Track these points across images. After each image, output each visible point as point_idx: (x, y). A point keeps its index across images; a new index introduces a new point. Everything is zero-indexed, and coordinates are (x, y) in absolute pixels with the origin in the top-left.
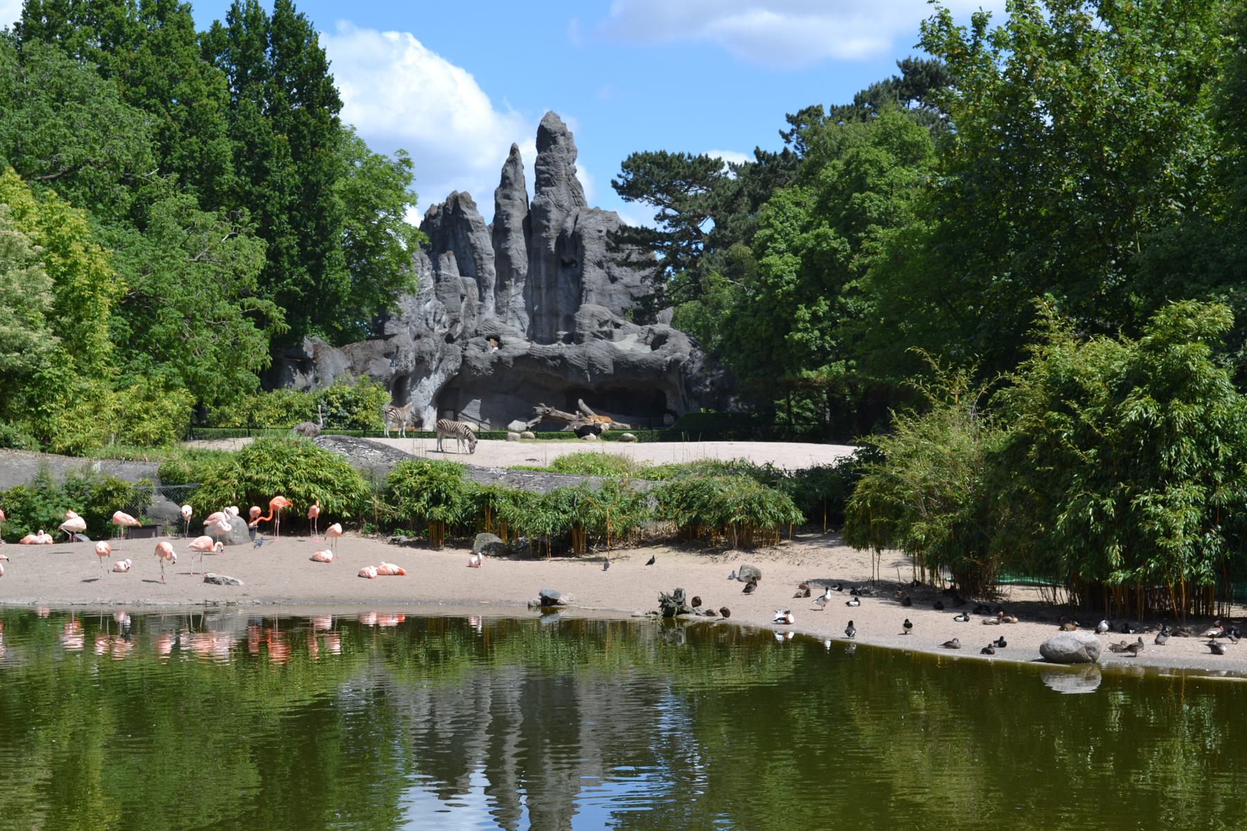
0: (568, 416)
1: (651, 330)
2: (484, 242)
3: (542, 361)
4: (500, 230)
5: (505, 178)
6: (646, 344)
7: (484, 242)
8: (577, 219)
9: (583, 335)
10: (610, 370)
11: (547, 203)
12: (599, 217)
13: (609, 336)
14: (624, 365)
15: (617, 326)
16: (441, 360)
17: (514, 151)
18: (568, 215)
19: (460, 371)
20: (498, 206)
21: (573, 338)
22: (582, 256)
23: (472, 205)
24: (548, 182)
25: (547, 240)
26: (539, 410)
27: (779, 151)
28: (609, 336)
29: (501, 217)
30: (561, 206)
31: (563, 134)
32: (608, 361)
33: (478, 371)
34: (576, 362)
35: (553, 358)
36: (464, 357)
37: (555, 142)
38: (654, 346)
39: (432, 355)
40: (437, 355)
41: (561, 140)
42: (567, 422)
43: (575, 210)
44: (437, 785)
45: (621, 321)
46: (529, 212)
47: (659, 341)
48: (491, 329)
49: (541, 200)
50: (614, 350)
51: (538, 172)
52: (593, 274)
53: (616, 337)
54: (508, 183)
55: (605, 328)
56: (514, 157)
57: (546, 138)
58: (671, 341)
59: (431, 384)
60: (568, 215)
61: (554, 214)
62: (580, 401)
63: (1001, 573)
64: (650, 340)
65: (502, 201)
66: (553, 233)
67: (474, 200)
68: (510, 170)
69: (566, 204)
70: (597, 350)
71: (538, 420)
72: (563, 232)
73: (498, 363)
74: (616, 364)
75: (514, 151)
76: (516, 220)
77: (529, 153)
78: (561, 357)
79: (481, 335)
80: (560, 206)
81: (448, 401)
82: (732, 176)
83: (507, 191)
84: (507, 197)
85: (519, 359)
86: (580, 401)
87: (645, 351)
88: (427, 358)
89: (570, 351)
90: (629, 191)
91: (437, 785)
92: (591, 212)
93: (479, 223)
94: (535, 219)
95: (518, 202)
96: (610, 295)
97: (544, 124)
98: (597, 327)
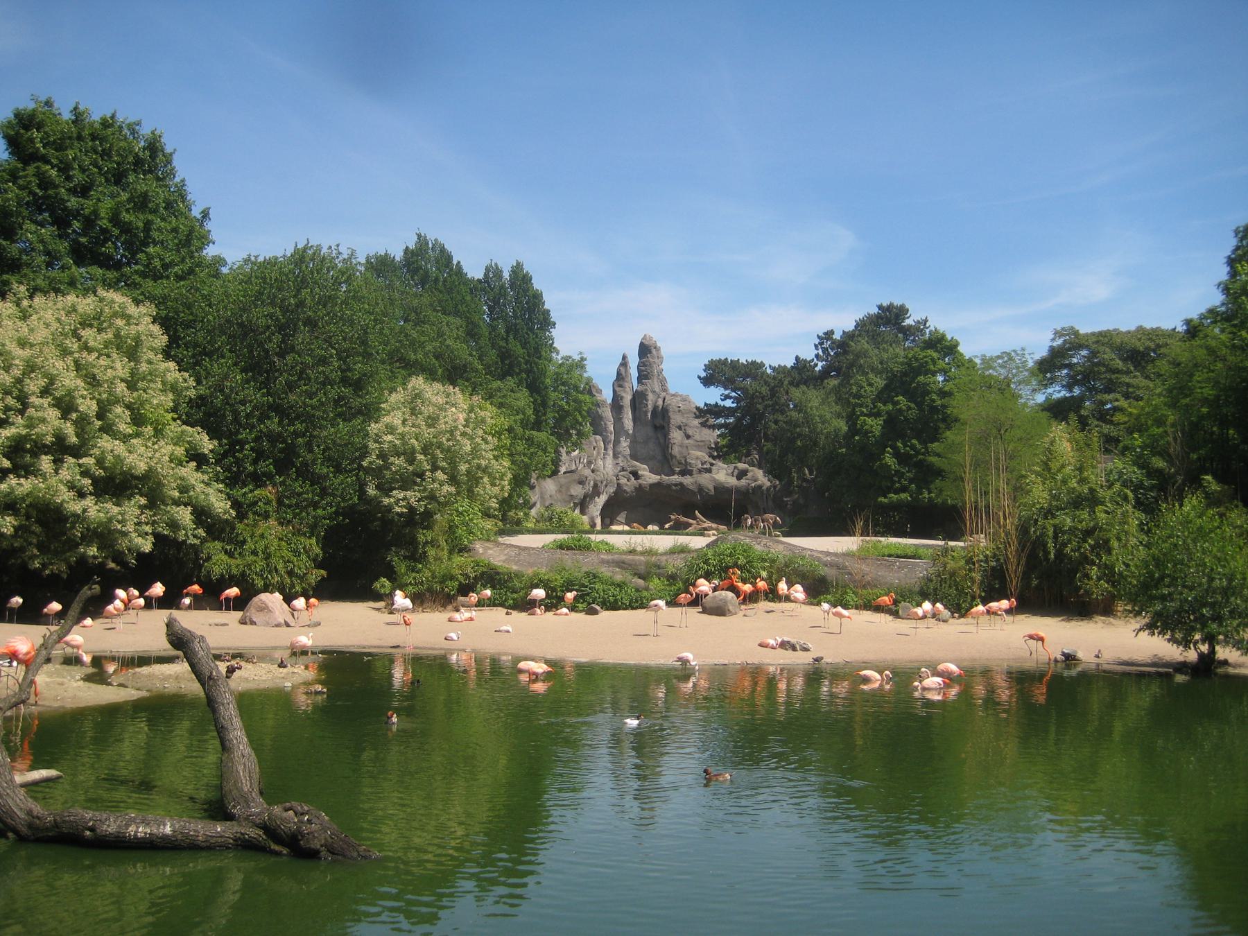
0: (691, 521)
1: (735, 468)
2: (607, 413)
3: (669, 486)
4: (617, 405)
5: (619, 374)
6: (733, 476)
7: (607, 413)
8: (664, 399)
9: (692, 471)
10: (712, 492)
11: (646, 390)
12: (679, 398)
13: (709, 471)
14: (721, 490)
15: (712, 465)
16: (606, 486)
17: (624, 357)
18: (659, 397)
19: (615, 493)
20: (614, 391)
21: (684, 473)
22: (669, 423)
23: (600, 391)
24: (647, 377)
25: (646, 413)
26: (673, 517)
27: (813, 356)
28: (709, 471)
29: (617, 399)
30: (655, 392)
31: (655, 348)
32: (711, 487)
33: (627, 493)
34: (692, 487)
35: (676, 485)
36: (618, 484)
37: (650, 352)
38: (739, 478)
39: (602, 483)
40: (605, 483)
41: (654, 351)
42: (690, 525)
43: (663, 394)
44: (1126, 833)
45: (714, 462)
46: (634, 395)
47: (741, 475)
48: (632, 466)
49: (641, 388)
50: (714, 480)
51: (639, 371)
52: (675, 433)
53: (713, 472)
54: (620, 378)
55: (705, 466)
56: (624, 363)
57: (645, 350)
58: (749, 475)
59: (601, 501)
60: (659, 397)
61: (651, 397)
62: (697, 512)
63: (1190, 635)
64: (736, 473)
65: (618, 389)
66: (650, 407)
67: (600, 387)
68: (623, 370)
69: (657, 390)
70: (705, 480)
71: (672, 523)
72: (655, 408)
73: (639, 489)
74: (715, 488)
75: (624, 357)
76: (627, 398)
77: (634, 361)
78: (681, 484)
79: (626, 470)
80: (654, 392)
81: (609, 514)
82: (769, 371)
83: (621, 383)
84: (620, 386)
85: (652, 486)
86: (697, 512)
87: (732, 481)
88: (599, 484)
89: (687, 480)
90: (707, 381)
91: (1126, 833)
92: (673, 395)
93: (604, 402)
94: (638, 399)
95: (628, 389)
96: (687, 447)
97: (643, 341)
98: (700, 466)
